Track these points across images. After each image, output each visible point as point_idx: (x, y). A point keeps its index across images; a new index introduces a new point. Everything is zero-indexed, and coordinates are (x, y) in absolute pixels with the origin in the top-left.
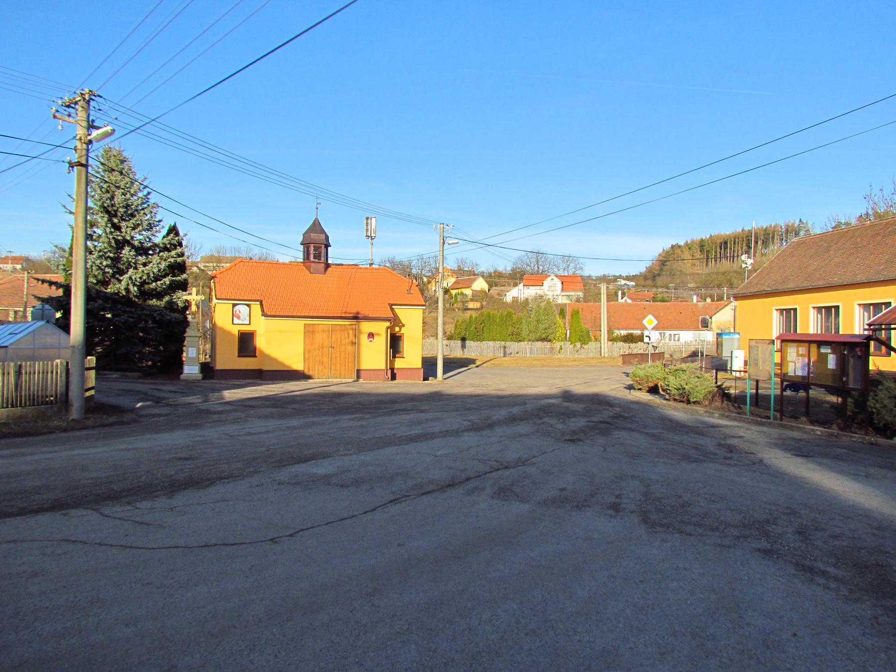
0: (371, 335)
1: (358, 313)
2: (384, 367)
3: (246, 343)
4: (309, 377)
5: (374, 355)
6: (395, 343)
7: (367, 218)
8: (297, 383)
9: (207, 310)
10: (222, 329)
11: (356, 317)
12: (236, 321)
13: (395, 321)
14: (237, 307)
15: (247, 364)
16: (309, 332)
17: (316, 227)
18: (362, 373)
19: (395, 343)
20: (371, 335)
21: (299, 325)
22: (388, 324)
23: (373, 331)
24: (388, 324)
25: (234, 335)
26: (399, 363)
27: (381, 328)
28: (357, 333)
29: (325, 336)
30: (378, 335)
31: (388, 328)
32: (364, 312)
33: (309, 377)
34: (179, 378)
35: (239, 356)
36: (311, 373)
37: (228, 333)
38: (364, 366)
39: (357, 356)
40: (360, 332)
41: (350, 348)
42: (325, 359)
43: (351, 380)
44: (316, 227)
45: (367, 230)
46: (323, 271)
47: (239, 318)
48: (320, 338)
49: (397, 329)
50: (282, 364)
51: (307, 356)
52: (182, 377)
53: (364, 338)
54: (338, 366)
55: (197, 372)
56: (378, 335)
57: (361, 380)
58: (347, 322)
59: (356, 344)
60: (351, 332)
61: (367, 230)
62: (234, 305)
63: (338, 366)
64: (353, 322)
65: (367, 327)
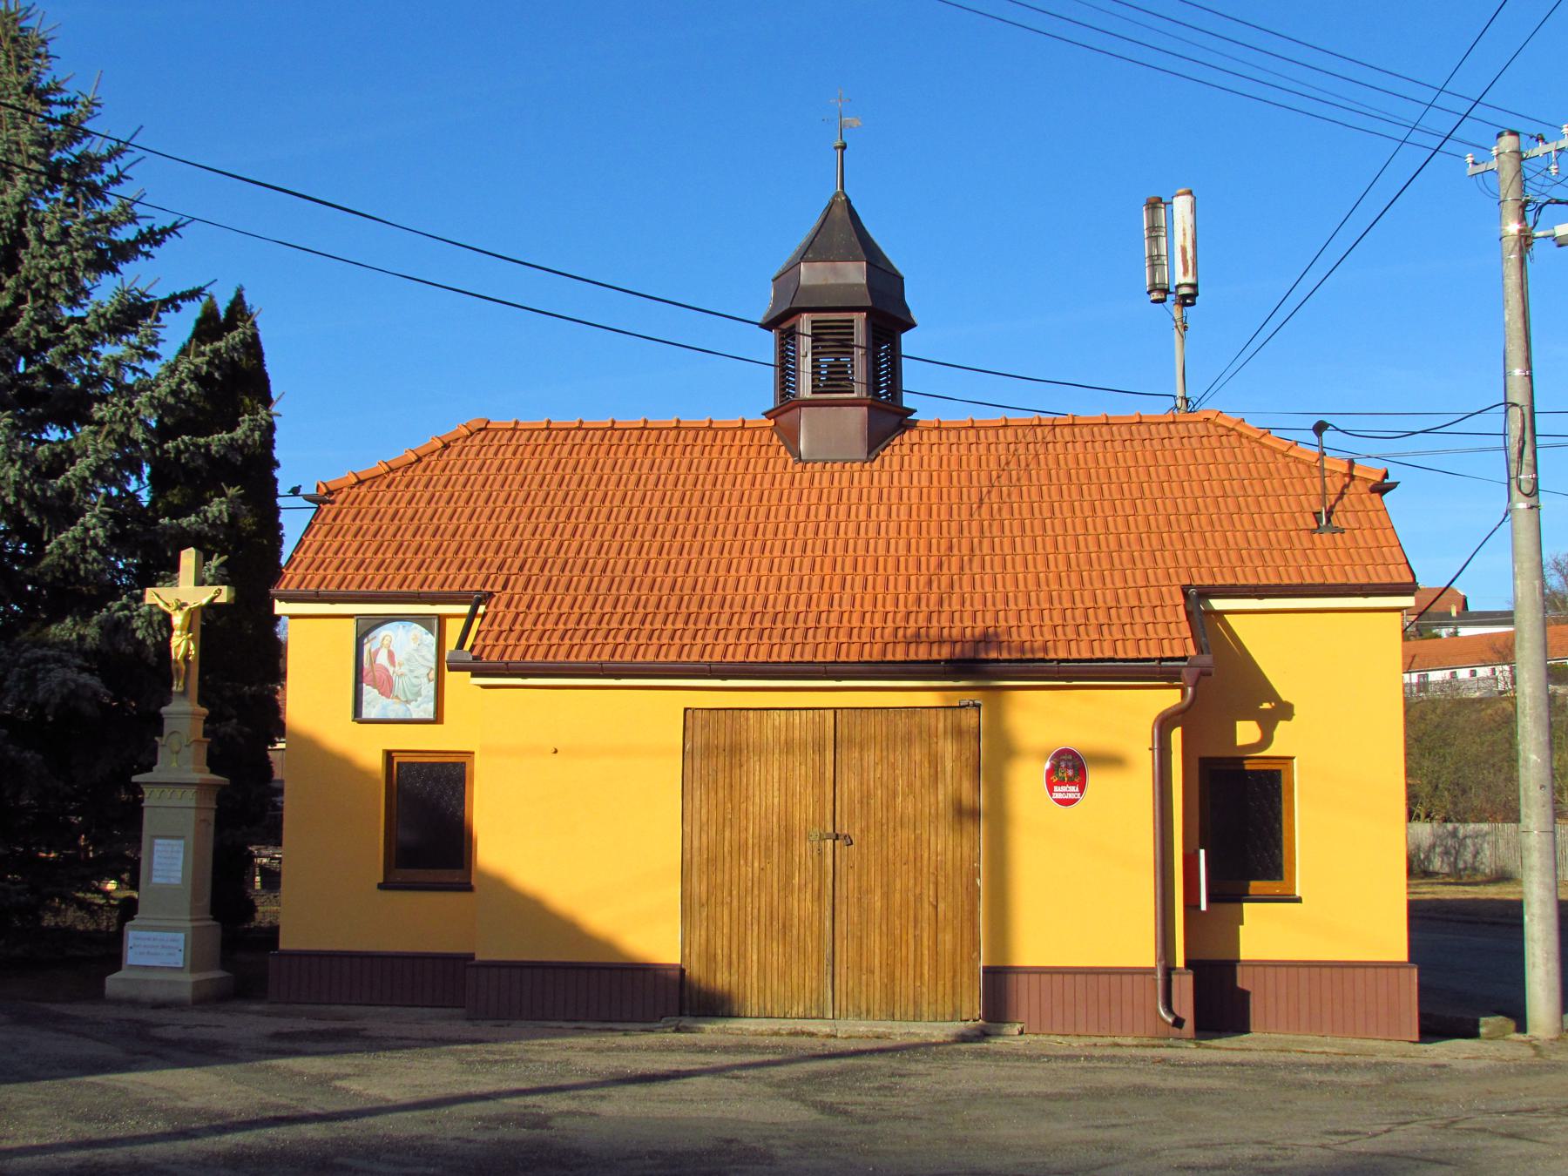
0: (1070, 768)
1: (986, 640)
2: (1144, 954)
3: (427, 814)
4: (715, 1006)
5: (1087, 883)
6: (1235, 824)
7: (1154, 205)
8: (1461, 896)
9: (245, 654)
10: (310, 747)
11: (979, 665)
12: (374, 704)
13: (1218, 689)
14: (384, 632)
15: (420, 923)
16: (712, 752)
17: (843, 231)
18: (1024, 996)
19: (1235, 824)
20: (1070, 768)
21: (654, 714)
22: (1170, 698)
23: (1078, 739)
24: (1170, 698)
25: (362, 774)
26: (1263, 933)
27: (1126, 719)
28: (989, 756)
29: (801, 771)
30: (1112, 761)
31: (1165, 723)
32: (1028, 632)
33: (715, 1006)
34: (95, 993)
35: (384, 886)
36: (723, 980)
37: (337, 766)
38: (1034, 946)
39: (989, 891)
40: (1006, 750)
41: (942, 842)
42: (803, 905)
43: (939, 1031)
44: (843, 231)
45: (1155, 262)
46: (860, 450)
47: (386, 688)
48: (770, 787)
49: (1246, 732)
50: (567, 928)
51: (699, 888)
52: (114, 983)
53: (1027, 782)
54: (875, 942)
55: (178, 960)
56: (1112, 761)
57: (1012, 1037)
58: (925, 697)
59: (981, 815)
60: (948, 748)
61: (1155, 262)
62: (367, 626)
63: (875, 942)
64: (959, 692)
65: (1042, 718)
